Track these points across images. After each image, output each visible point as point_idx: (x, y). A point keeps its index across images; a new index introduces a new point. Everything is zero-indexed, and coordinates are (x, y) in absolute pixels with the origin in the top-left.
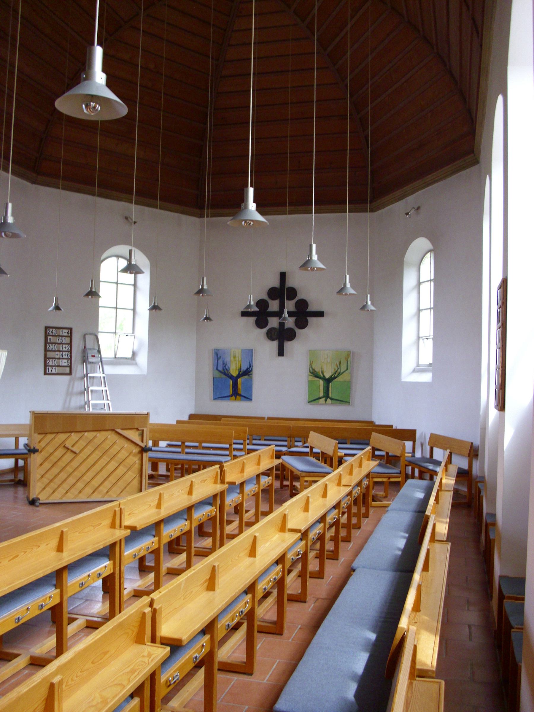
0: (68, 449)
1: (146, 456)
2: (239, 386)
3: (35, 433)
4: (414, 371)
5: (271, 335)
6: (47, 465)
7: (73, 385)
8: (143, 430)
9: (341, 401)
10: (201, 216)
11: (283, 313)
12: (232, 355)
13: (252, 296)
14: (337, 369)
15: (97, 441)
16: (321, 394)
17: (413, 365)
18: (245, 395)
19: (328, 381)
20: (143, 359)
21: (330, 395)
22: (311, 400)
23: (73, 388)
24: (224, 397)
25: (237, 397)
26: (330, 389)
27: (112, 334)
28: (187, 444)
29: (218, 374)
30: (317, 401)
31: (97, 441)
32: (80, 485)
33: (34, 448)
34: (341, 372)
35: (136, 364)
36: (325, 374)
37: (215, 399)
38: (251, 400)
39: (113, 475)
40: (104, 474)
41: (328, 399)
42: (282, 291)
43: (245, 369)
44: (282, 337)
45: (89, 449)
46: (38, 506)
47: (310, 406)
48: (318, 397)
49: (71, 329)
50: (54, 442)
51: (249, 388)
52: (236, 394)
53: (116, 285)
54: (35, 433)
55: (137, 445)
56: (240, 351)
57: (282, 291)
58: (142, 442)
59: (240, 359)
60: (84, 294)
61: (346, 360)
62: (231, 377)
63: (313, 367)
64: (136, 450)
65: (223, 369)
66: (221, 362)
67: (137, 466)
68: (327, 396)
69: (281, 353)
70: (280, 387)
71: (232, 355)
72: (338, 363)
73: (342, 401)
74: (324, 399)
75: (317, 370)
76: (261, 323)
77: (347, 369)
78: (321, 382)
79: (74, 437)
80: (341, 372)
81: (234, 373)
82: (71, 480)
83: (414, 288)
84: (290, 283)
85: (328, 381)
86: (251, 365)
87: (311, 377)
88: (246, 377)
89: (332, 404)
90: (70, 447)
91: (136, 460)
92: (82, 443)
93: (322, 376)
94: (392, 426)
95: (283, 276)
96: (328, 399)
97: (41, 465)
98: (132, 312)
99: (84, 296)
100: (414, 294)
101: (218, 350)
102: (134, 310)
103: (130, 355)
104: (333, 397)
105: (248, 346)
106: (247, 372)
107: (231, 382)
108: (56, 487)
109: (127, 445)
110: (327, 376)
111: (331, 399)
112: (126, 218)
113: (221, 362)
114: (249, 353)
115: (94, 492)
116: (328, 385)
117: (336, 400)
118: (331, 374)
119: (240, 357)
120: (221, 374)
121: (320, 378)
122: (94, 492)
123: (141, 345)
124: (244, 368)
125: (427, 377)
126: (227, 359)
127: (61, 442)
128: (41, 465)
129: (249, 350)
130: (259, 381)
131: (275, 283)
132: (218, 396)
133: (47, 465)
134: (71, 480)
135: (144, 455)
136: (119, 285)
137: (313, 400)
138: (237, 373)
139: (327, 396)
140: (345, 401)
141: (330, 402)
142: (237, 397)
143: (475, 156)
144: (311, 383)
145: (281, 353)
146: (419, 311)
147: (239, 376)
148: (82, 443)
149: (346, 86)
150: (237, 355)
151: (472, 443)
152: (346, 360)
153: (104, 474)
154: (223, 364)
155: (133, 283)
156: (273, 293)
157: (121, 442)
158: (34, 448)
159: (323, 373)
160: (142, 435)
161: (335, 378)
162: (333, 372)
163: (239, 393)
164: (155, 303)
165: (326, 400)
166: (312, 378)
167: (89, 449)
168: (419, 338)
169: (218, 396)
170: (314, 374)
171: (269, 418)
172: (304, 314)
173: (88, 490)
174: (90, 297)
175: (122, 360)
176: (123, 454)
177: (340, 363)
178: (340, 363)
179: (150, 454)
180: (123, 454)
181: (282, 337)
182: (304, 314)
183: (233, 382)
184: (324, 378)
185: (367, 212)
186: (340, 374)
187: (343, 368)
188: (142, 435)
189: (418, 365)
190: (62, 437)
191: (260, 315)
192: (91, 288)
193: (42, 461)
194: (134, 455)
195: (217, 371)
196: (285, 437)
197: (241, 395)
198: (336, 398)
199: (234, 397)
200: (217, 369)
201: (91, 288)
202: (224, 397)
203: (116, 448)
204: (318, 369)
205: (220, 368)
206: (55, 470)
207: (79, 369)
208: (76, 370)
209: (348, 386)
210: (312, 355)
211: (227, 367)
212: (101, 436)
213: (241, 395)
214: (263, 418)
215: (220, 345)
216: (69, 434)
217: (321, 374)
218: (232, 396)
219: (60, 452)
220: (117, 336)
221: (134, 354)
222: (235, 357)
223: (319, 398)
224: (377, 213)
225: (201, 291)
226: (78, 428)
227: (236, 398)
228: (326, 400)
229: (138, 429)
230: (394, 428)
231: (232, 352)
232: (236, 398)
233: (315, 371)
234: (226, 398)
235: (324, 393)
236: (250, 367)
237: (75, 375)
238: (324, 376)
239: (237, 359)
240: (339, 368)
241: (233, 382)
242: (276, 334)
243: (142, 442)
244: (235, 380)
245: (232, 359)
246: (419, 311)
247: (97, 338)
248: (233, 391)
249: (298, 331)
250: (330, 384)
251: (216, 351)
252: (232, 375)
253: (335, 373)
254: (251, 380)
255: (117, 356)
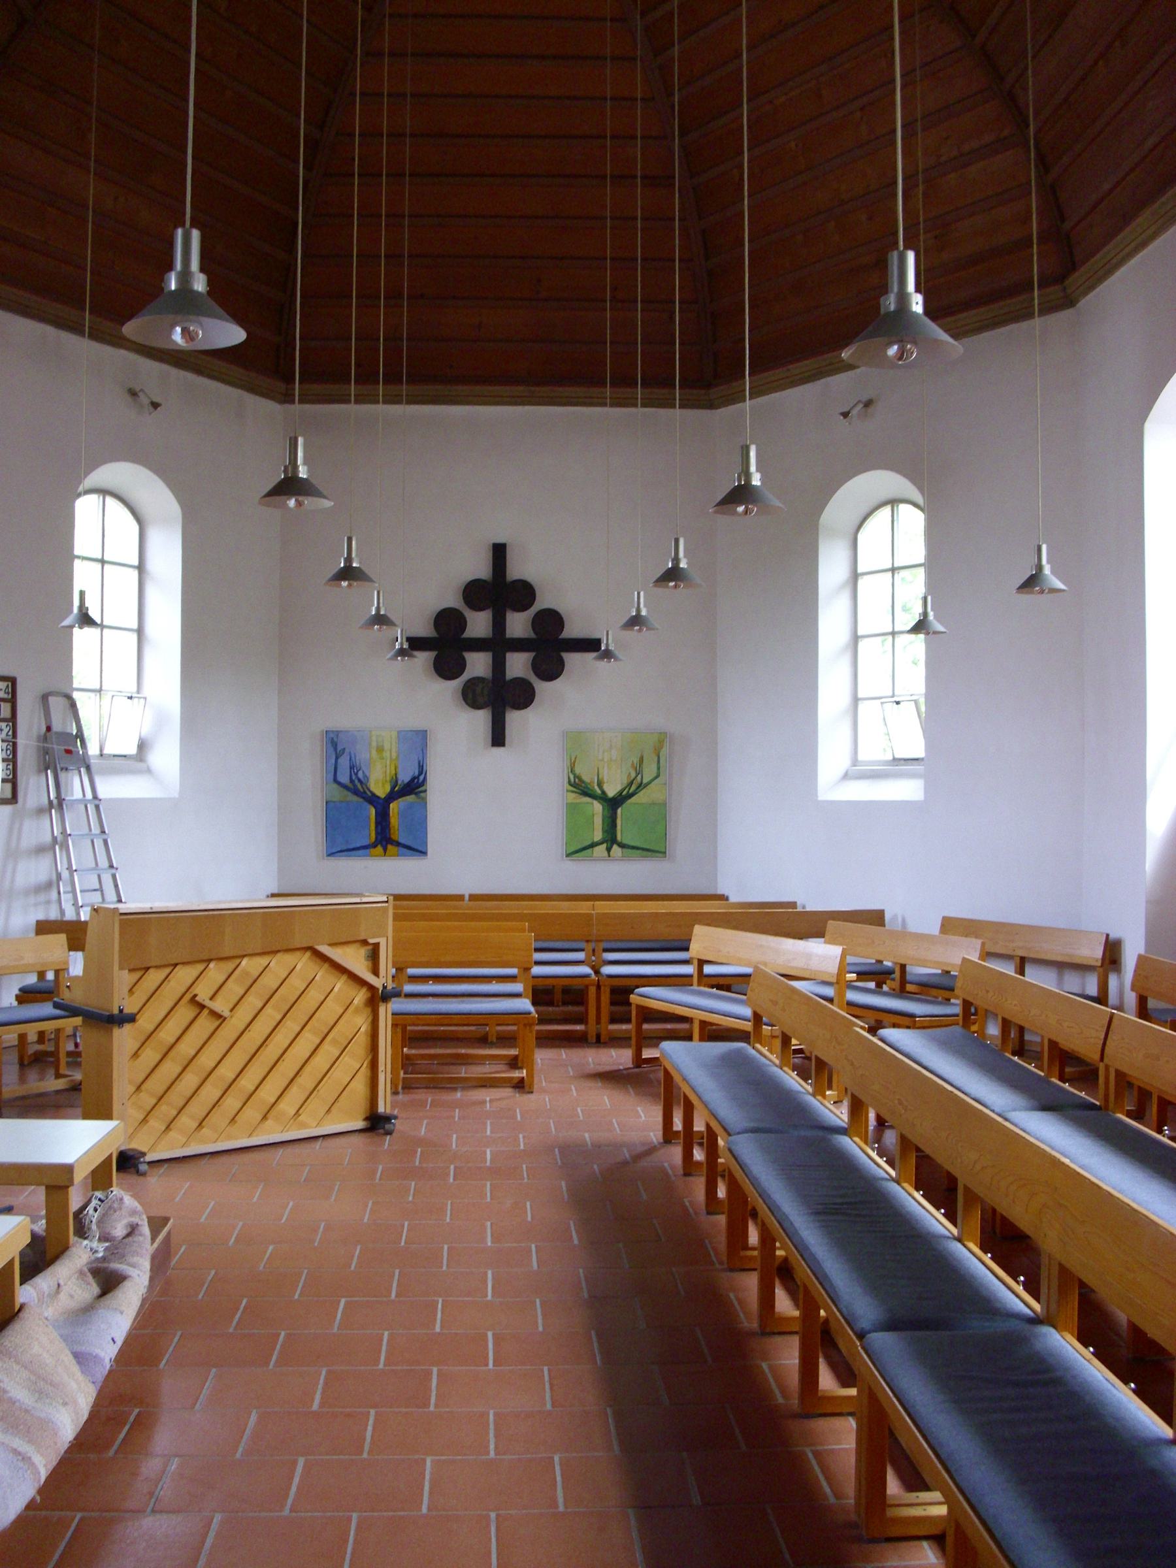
0: (202, 1007)
1: (385, 1012)
2: (394, 821)
3: (121, 968)
4: (846, 776)
5: (472, 696)
6: (150, 1055)
7: (21, 825)
8: (376, 947)
9: (643, 849)
10: (286, 398)
11: (500, 642)
12: (374, 744)
13: (642, 594)
14: (633, 775)
15: (269, 982)
16: (598, 836)
17: (845, 763)
18: (408, 843)
19: (613, 804)
20: (167, 758)
21: (619, 838)
22: (573, 849)
23: (19, 839)
24: (354, 849)
25: (390, 847)
26: (619, 822)
27: (92, 695)
28: (411, 971)
29: (338, 794)
30: (589, 851)
31: (269, 982)
32: (232, 1103)
33: (121, 1011)
34: (645, 781)
35: (149, 771)
36: (605, 787)
37: (329, 855)
38: (423, 853)
39: (308, 1068)
40: (288, 1067)
41: (615, 847)
42: (500, 589)
43: (407, 779)
44: (500, 700)
45: (253, 1001)
46: (144, 1174)
47: (570, 865)
48: (588, 843)
49: (13, 681)
50: (166, 988)
51: (419, 825)
52: (383, 840)
53: (100, 566)
54: (121, 968)
55: (362, 982)
56: (394, 734)
57: (500, 589)
58: (375, 972)
59: (394, 755)
60: (330, 575)
61: (655, 755)
62: (372, 799)
63: (577, 771)
64: (361, 996)
65: (352, 781)
66: (344, 762)
67: (362, 1039)
68: (611, 838)
69: (498, 738)
70: (499, 821)
71: (374, 744)
72: (636, 760)
73: (648, 850)
74: (605, 845)
75: (586, 778)
76: (447, 668)
77: (658, 776)
78: (598, 807)
79: (216, 973)
80: (645, 781)
81: (381, 789)
82: (211, 1092)
83: (842, 587)
84: (516, 570)
85: (613, 804)
86: (422, 769)
87: (574, 795)
88: (411, 798)
89: (624, 858)
90: (207, 1003)
91: (361, 1022)
92: (234, 989)
93: (599, 792)
94: (793, 905)
95: (499, 552)
96: (615, 847)
97: (136, 1055)
98: (134, 637)
99: (326, 584)
100: (844, 601)
101: (338, 733)
102: (140, 631)
103: (132, 750)
104: (625, 842)
105: (413, 722)
106: (414, 787)
107: (373, 811)
108: (175, 1113)
109: (341, 984)
110: (611, 793)
111: (622, 846)
112: (133, 393)
113: (344, 762)
114: (419, 741)
115: (265, 1117)
116: (612, 813)
117: (633, 848)
118: (619, 788)
119: (394, 750)
120: (346, 792)
121: (593, 796)
122: (265, 1117)
123: (160, 721)
124: (404, 777)
125: (909, 790)
126: (362, 756)
127: (183, 990)
128: (136, 1055)
129: (417, 732)
130: (446, 810)
131: (481, 569)
132: (339, 845)
133: (150, 1055)
134: (211, 1092)
135: (382, 1009)
136: (106, 566)
137: (579, 851)
138: (388, 789)
139: (611, 838)
140: (654, 850)
141: (620, 854)
142: (390, 847)
143: (1065, 289)
144: (572, 809)
145: (498, 738)
146: (856, 638)
147: (392, 796)
148: (234, 989)
149: (673, 106)
150: (387, 746)
151: (1108, 935)
152: (655, 755)
153: (288, 1067)
154: (352, 767)
155: (136, 563)
156: (475, 593)
157: (323, 975)
158: (121, 1011)
159: (600, 784)
160: (374, 955)
161: (630, 796)
162: (625, 782)
163: (394, 837)
164: (378, 609)
165: (609, 850)
166: (572, 797)
167: (253, 1001)
168: (856, 700)
169: (339, 845)
170: (580, 787)
171: (473, 897)
172: (553, 645)
173: (252, 1114)
174: (345, 584)
175: (117, 761)
176: (332, 1008)
177: (641, 760)
178: (641, 760)
179: (396, 1005)
180: (332, 1008)
181: (500, 700)
182: (553, 645)
183: (377, 811)
184: (603, 798)
185: (674, 407)
186: (641, 786)
187: (648, 773)
188: (374, 955)
189: (855, 762)
190: (185, 975)
191: (443, 645)
192: (349, 559)
193: (137, 1045)
194: (357, 1010)
195: (335, 786)
196: (581, 940)
197: (398, 844)
198: (633, 844)
199: (379, 849)
200: (335, 780)
201: (349, 559)
202: (354, 849)
203: (314, 996)
204: (588, 776)
205: (344, 778)
206: (170, 1068)
207: (36, 788)
208: (26, 789)
209: (660, 814)
210: (575, 743)
211: (360, 775)
212: (279, 965)
213: (398, 844)
214: (460, 898)
215: (347, 717)
216: (200, 967)
217: (596, 787)
218: (374, 846)
219: (185, 1013)
220: (106, 698)
221: (142, 746)
222: (380, 749)
223: (593, 845)
224: (719, 411)
225: (673, 575)
226: (228, 952)
227: (385, 850)
228: (609, 850)
229: (365, 942)
230: (799, 909)
231: (374, 738)
232: (385, 850)
233: (583, 782)
234: (361, 852)
235: (604, 831)
236: (420, 773)
237: (24, 804)
238: (604, 792)
239: (387, 754)
240: (639, 772)
241: (377, 811)
242: (486, 692)
243: (375, 972)
244: (382, 806)
245: (374, 752)
246: (856, 638)
247: (73, 705)
248: (377, 833)
249: (456, 684)
250: (619, 811)
251: (332, 735)
252: (373, 794)
253: (631, 783)
254: (424, 804)
255: (106, 752)
